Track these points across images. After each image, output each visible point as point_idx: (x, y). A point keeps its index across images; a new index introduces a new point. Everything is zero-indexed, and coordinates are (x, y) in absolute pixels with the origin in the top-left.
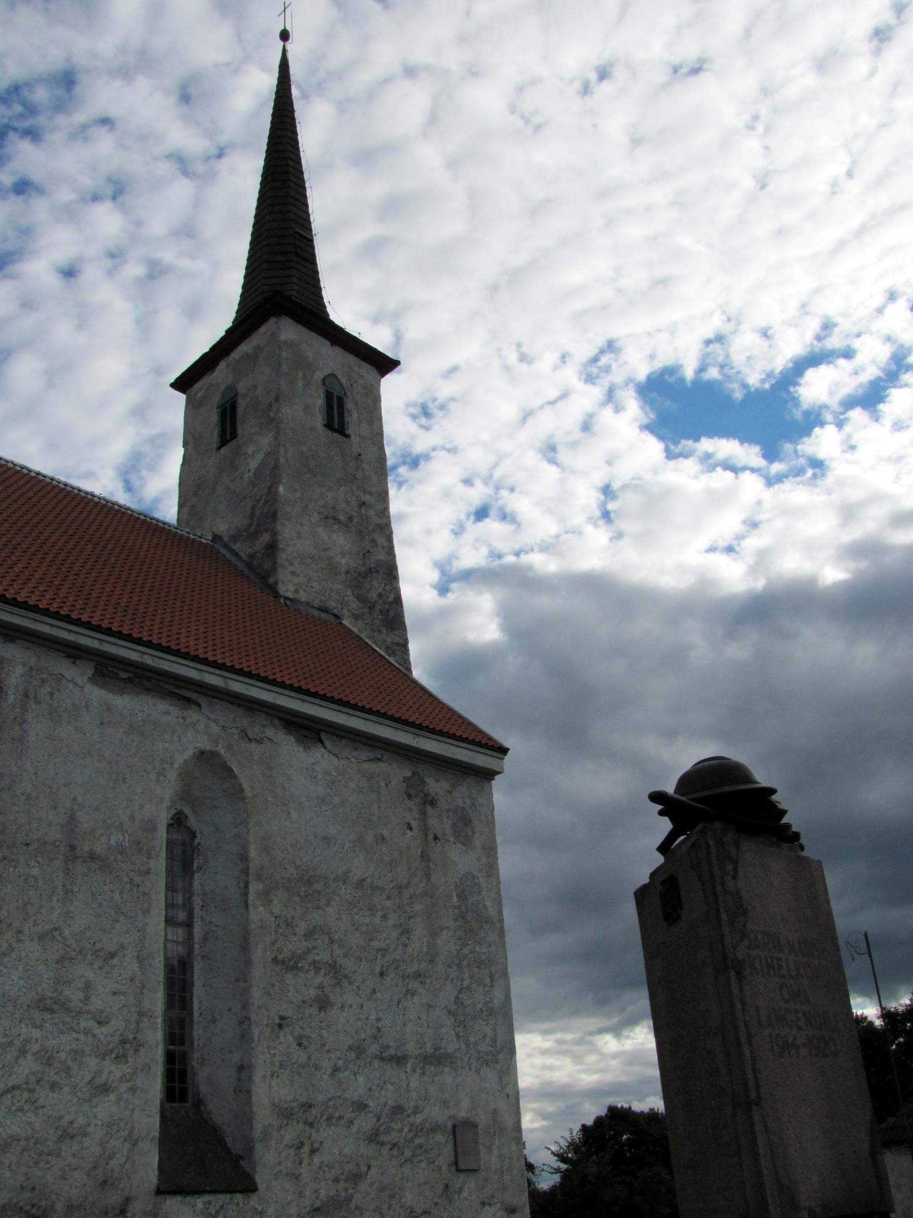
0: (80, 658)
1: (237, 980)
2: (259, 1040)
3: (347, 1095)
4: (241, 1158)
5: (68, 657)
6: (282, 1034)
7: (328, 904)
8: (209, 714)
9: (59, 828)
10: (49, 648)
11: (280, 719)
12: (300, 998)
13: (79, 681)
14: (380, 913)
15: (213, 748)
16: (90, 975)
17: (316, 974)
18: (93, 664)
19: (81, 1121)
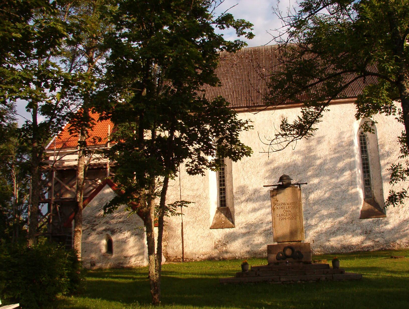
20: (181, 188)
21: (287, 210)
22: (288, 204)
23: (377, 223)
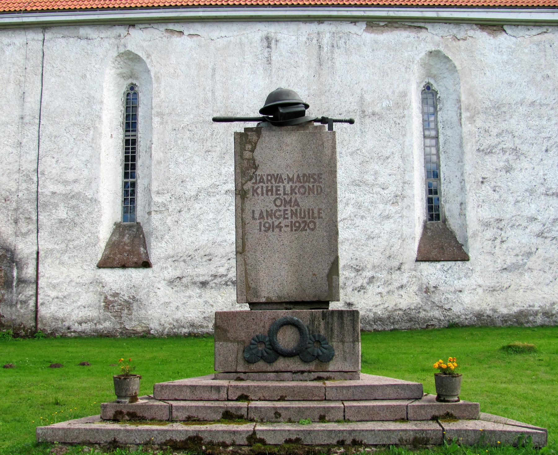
0: (358, 22)
1: (459, 162)
2: (470, 190)
3: (524, 214)
5: (352, 23)
6: (483, 186)
7: (511, 117)
8: (433, 32)
11: (476, 24)
12: (494, 167)
13: (359, 33)
14: (546, 118)
15: (436, 49)
16: (377, 168)
17: (503, 154)
18: (365, 23)
19: (377, 231)
20: (39, 176)
21: (288, 199)
22: (290, 180)
23: (450, 271)
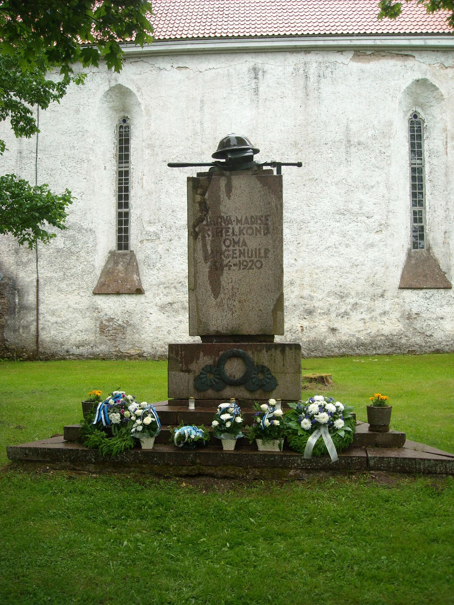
0: (344, 51)
4: (445, 273)
9: (341, 134)
10: (328, 51)
19: (361, 259)
